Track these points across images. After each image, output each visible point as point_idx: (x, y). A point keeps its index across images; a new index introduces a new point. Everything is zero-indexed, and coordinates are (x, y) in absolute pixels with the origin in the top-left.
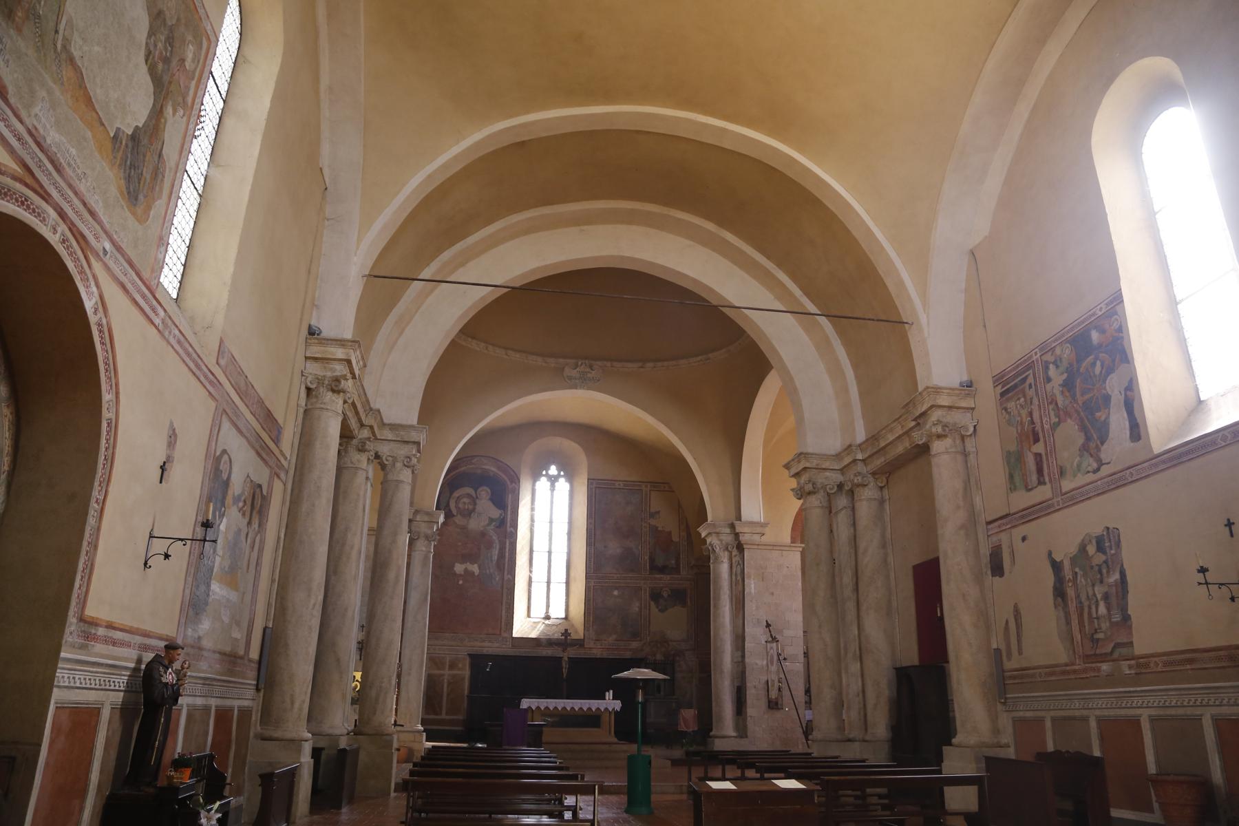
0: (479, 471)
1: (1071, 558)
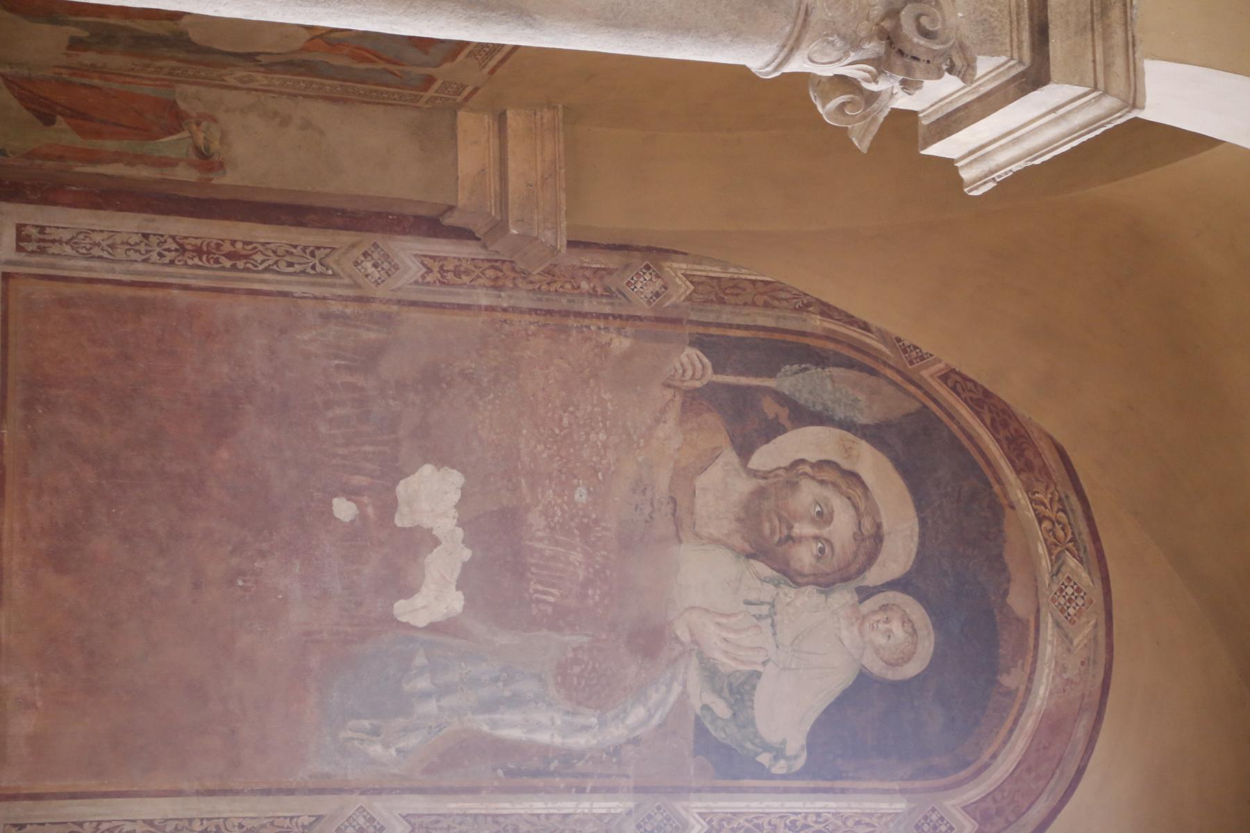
0: (1018, 602)
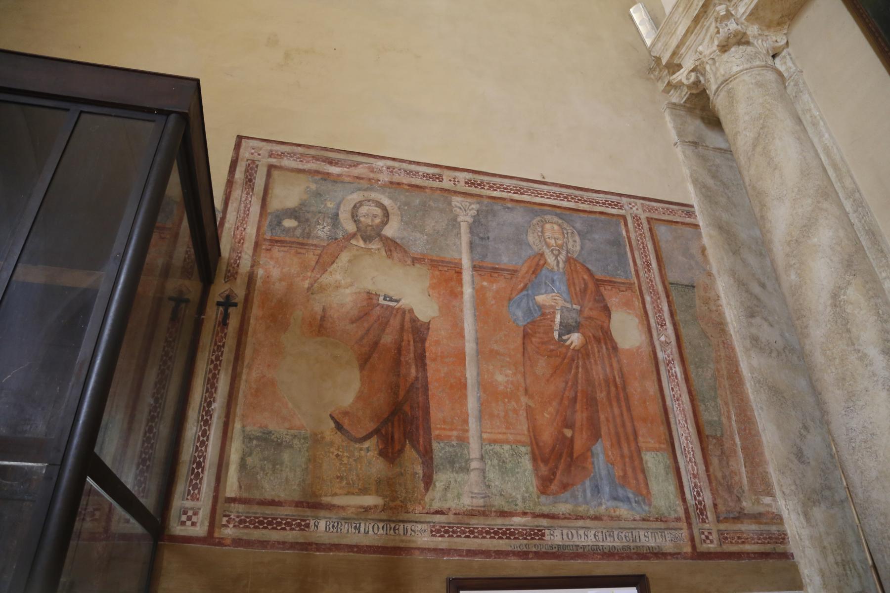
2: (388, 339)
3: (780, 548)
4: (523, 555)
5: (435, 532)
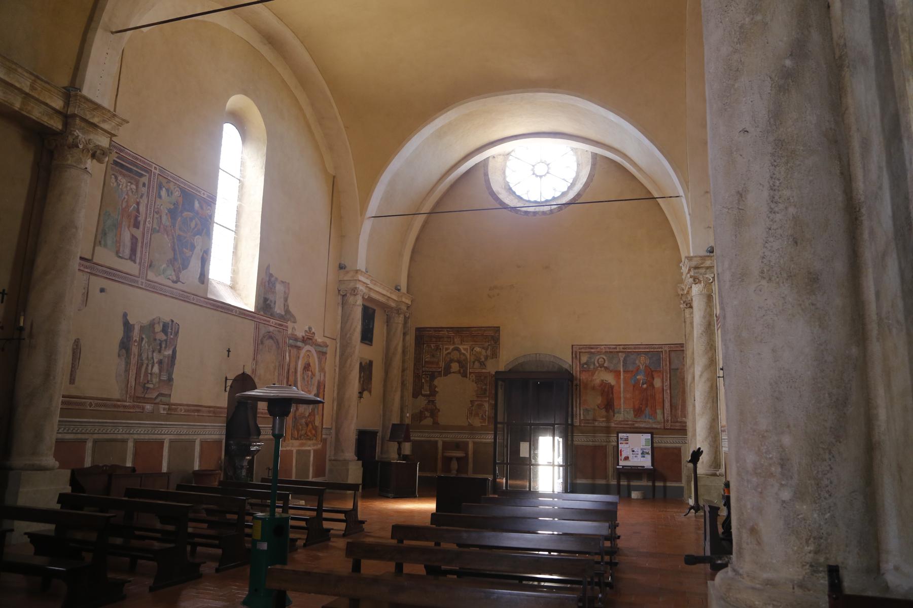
1: (141, 326)
2: (606, 390)
3: (685, 428)
4: (630, 428)
5: (615, 424)
